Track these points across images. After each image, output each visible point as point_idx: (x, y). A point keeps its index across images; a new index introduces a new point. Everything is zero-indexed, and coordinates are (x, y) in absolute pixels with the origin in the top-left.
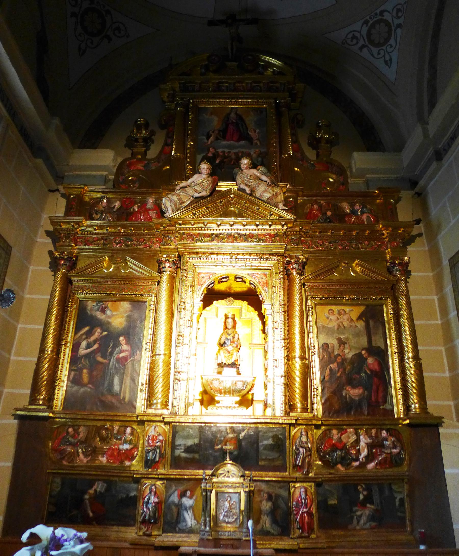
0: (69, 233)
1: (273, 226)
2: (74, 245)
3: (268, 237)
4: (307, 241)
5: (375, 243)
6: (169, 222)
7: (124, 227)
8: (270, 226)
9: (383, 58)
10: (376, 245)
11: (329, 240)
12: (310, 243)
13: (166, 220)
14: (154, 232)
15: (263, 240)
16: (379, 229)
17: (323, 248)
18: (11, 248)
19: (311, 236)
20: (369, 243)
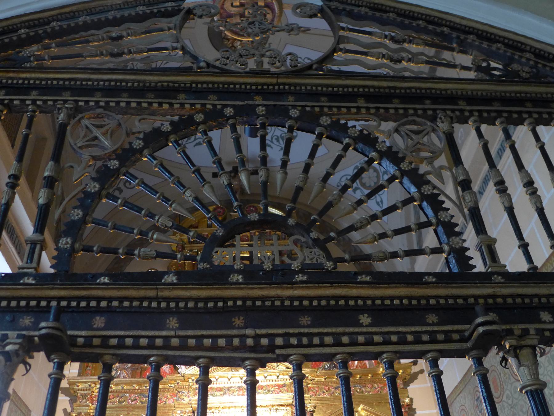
0: (86, 392)
1: (281, 377)
2: (91, 405)
3: (277, 387)
4: (313, 388)
5: (378, 385)
6: (182, 378)
7: (139, 384)
8: (278, 377)
9: (375, 200)
10: (379, 387)
11: (335, 386)
12: (317, 390)
13: (179, 375)
14: (168, 387)
15: (272, 391)
16: (380, 372)
17: (329, 394)
18: (31, 411)
19: (317, 383)
20: (372, 386)
